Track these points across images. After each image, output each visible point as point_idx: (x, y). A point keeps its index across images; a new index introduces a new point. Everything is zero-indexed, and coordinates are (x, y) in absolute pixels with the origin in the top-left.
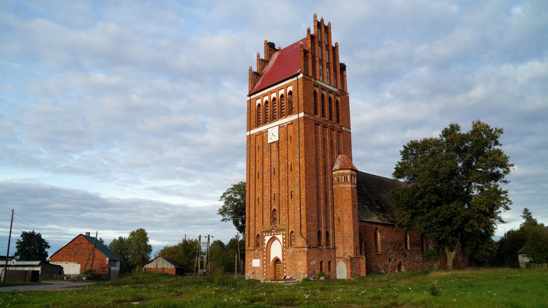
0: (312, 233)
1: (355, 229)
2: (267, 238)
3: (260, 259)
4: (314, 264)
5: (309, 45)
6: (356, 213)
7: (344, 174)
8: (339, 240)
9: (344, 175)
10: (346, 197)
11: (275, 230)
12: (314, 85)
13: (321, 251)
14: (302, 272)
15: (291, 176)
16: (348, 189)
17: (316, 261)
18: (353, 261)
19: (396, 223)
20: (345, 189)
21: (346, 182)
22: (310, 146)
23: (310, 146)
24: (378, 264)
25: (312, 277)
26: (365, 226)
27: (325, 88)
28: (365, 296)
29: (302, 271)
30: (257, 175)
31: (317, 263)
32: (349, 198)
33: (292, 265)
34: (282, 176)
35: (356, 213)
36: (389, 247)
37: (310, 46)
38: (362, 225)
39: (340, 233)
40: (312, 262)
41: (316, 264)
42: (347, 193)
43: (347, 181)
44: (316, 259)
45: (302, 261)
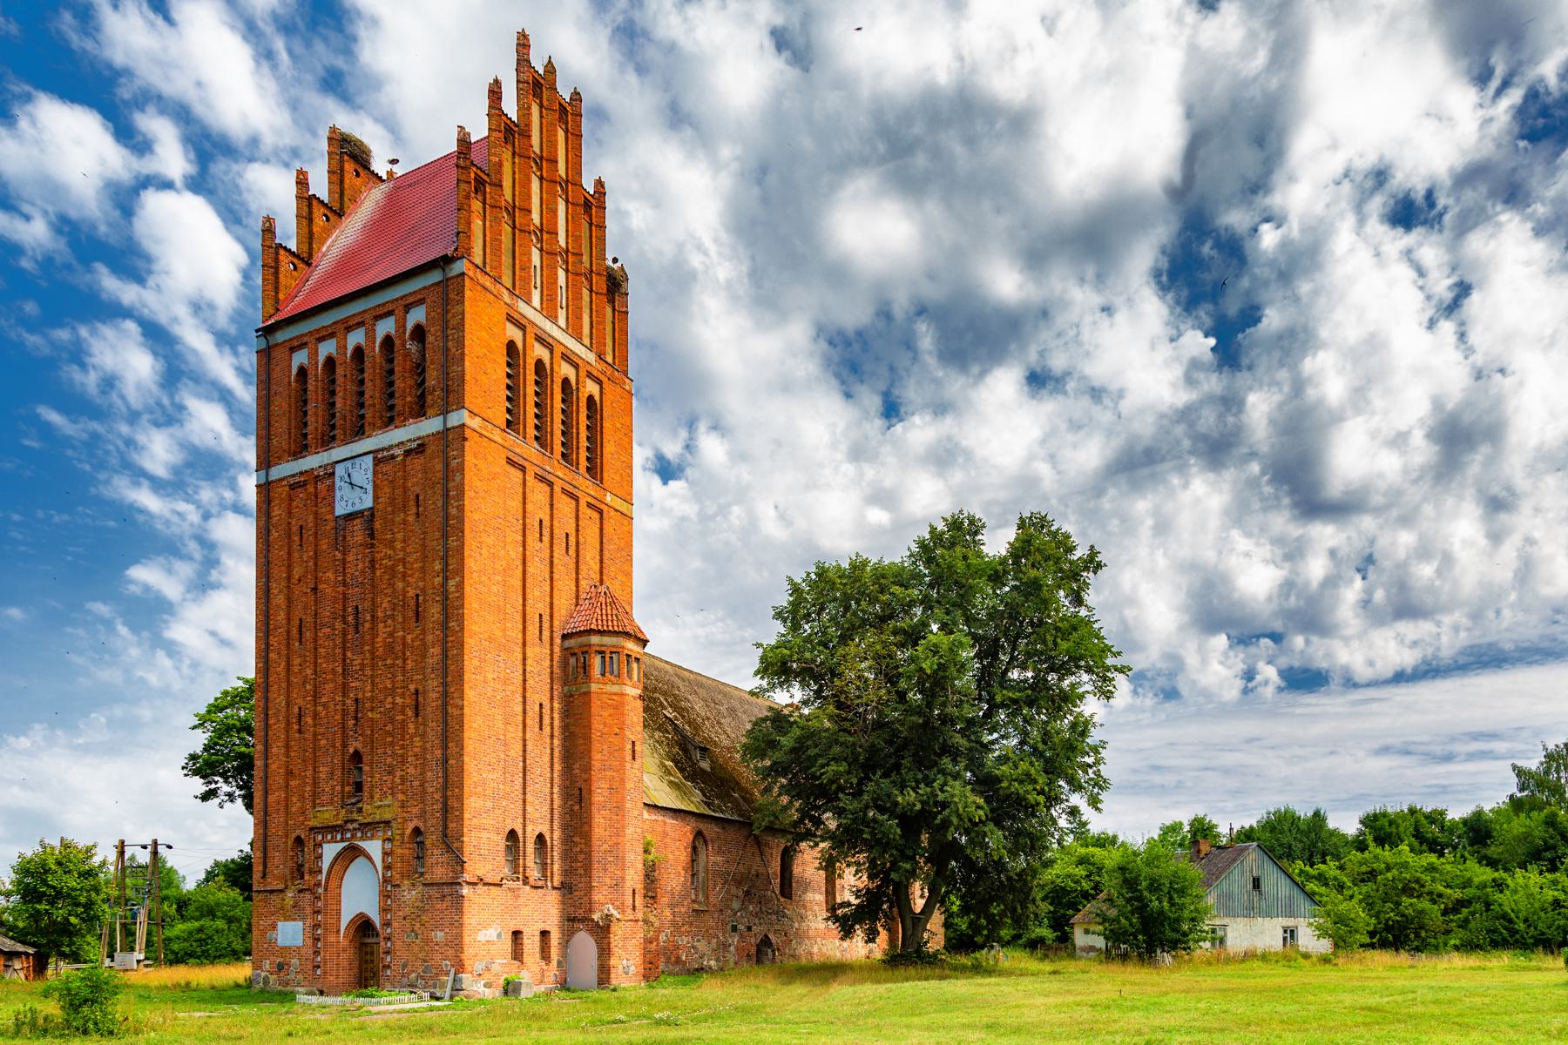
0: (484, 835)
2: (330, 851)
3: (303, 919)
10: (605, 724)
11: (356, 825)
12: (510, 319)
22: (485, 538)
30: (295, 631)
31: (499, 935)
40: (484, 931)
44: (498, 921)
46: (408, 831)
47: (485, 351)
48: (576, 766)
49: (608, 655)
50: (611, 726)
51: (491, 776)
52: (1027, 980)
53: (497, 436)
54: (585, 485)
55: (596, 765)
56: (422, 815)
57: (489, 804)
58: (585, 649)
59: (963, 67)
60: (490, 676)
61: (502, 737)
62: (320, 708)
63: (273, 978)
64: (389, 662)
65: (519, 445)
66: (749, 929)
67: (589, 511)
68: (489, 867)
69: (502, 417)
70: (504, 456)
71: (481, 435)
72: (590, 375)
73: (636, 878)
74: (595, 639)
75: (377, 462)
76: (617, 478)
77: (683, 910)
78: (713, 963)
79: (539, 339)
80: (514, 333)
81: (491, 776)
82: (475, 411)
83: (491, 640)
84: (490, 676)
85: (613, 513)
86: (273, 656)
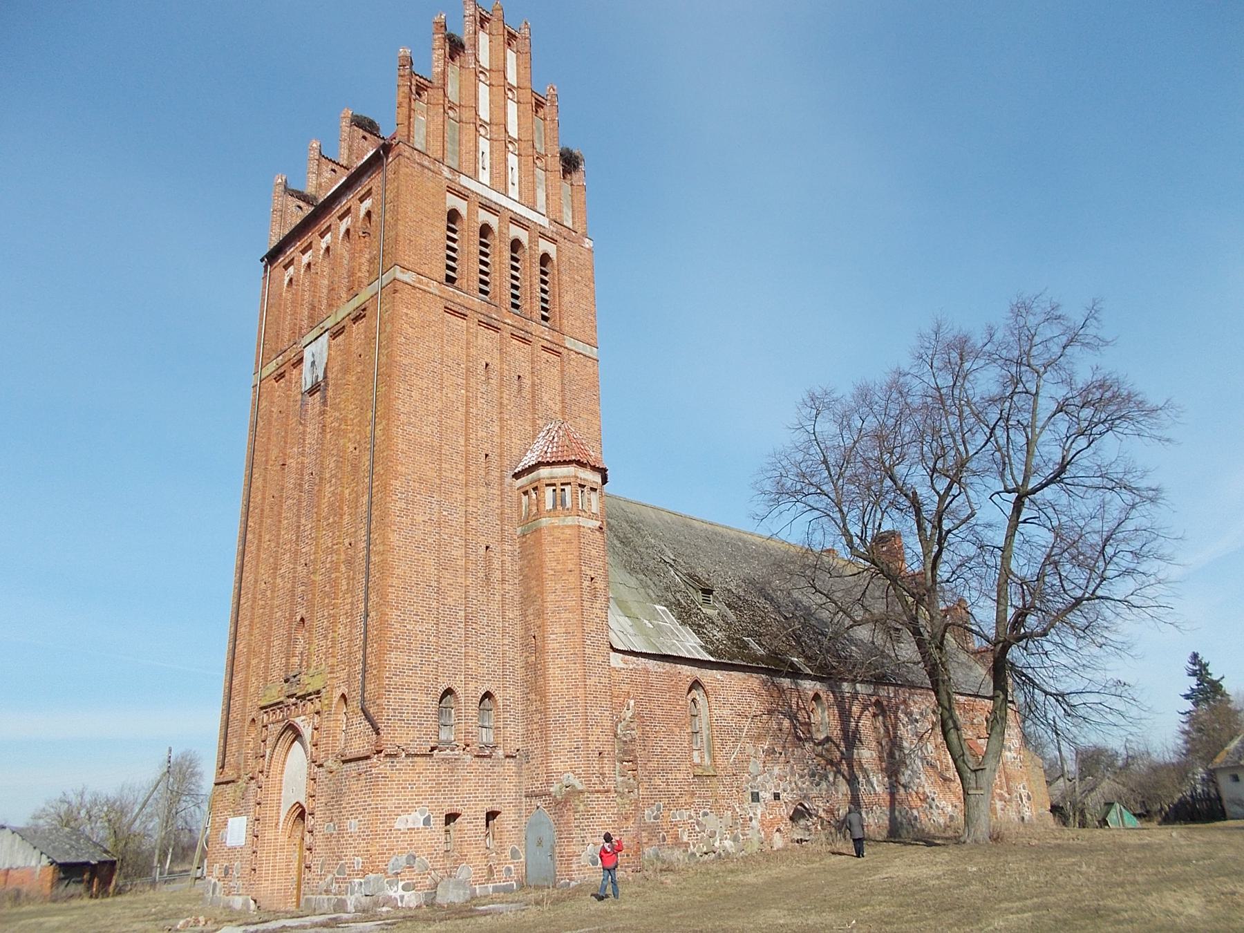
0: (408, 696)
1: (594, 679)
4: (410, 825)
5: (438, 66)
6: (597, 620)
7: (553, 481)
8: (535, 726)
9: (554, 485)
10: (558, 561)
12: (450, 190)
13: (452, 770)
14: (358, 863)
15: (353, 490)
16: (568, 531)
17: (422, 813)
18: (581, 808)
19: (1162, 903)
20: (557, 533)
21: (559, 508)
22: (415, 380)
23: (415, 380)
24: (705, 814)
25: (401, 884)
26: (647, 671)
27: (498, 208)
28: (923, 888)
29: (360, 859)
31: (427, 821)
32: (571, 567)
33: (331, 834)
34: (330, 495)
35: (597, 620)
36: (750, 749)
37: (439, 70)
38: (631, 667)
39: (538, 698)
40: (404, 817)
41: (421, 825)
42: (563, 546)
43: (563, 503)
44: (426, 802)
45: (360, 817)
46: (335, 700)
47: (420, 216)
48: (530, 611)
49: (559, 487)
50: (564, 564)
51: (418, 628)
52: (910, 847)
53: (433, 287)
54: (540, 330)
55: (550, 607)
56: (348, 682)
57: (415, 660)
58: (535, 485)
59: (1219, 681)
60: (419, 519)
61: (434, 584)
62: (279, 580)
63: (220, 884)
64: (331, 520)
65: (458, 296)
66: (777, 796)
67: (546, 355)
68: (414, 734)
69: (442, 273)
70: (442, 306)
71: (414, 287)
72: (543, 236)
73: (603, 738)
74: (544, 472)
75: (334, 336)
76: (578, 323)
77: (680, 776)
78: (728, 843)
79: (484, 207)
80: (453, 202)
81: (418, 628)
82: (407, 265)
83: (421, 480)
84: (419, 519)
85: (573, 356)
86: (249, 536)
